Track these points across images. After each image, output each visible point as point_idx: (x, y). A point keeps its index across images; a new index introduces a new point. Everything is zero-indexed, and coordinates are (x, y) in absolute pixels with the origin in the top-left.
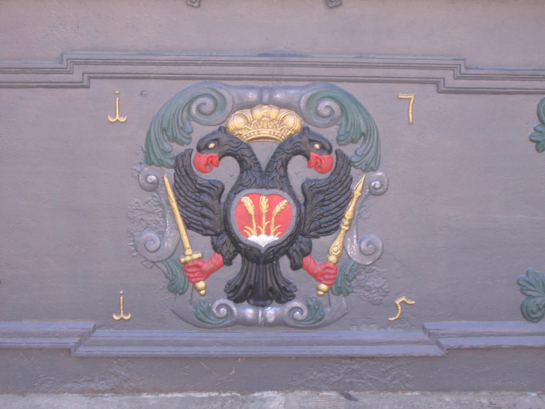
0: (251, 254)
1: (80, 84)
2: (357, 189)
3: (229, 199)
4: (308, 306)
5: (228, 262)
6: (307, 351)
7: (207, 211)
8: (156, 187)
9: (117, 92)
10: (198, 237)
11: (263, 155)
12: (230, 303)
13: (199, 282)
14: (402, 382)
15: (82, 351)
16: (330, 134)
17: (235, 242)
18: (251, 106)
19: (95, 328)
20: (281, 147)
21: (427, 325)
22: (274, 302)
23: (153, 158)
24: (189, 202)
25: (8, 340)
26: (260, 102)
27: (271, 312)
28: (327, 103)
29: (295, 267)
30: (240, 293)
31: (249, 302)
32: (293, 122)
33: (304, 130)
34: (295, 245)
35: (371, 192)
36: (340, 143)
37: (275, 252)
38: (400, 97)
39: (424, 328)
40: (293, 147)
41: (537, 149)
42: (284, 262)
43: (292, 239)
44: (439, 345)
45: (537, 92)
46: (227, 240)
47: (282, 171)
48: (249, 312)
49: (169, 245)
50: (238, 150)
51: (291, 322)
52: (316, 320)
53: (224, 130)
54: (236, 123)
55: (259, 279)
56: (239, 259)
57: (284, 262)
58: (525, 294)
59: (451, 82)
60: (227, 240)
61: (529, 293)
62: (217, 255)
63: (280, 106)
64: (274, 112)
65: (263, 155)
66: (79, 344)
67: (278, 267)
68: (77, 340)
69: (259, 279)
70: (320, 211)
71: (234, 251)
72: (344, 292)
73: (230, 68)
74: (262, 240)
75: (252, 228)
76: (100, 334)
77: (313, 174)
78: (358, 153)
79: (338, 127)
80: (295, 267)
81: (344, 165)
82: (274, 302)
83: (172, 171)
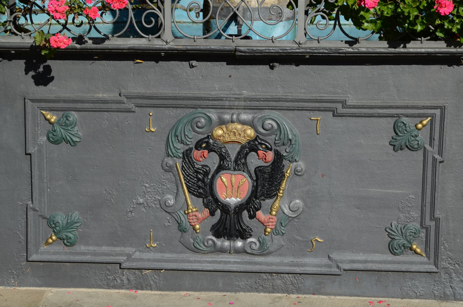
0: (225, 208)
3: (213, 177)
4: (259, 241)
7: (203, 186)
9: (151, 114)
12: (214, 238)
16: (271, 139)
17: (216, 200)
20: (243, 147)
21: (334, 256)
22: (239, 238)
23: (170, 153)
24: (190, 178)
28: (270, 122)
29: (252, 217)
30: (219, 231)
31: (224, 238)
32: (250, 132)
34: (250, 206)
35: (296, 173)
36: (277, 145)
37: (240, 208)
38: (312, 118)
39: (329, 257)
40: (253, 146)
41: (394, 150)
42: (245, 214)
44: (338, 267)
45: (392, 116)
46: (212, 202)
47: (243, 160)
48: (227, 244)
51: (249, 251)
52: (263, 251)
55: (230, 224)
58: (391, 238)
60: (212, 202)
61: (392, 237)
62: (206, 209)
63: (243, 123)
70: (267, 182)
71: (216, 207)
72: (281, 234)
74: (233, 200)
77: (261, 163)
78: (287, 151)
79: (275, 136)
80: (252, 217)
82: (239, 238)
83: (182, 160)
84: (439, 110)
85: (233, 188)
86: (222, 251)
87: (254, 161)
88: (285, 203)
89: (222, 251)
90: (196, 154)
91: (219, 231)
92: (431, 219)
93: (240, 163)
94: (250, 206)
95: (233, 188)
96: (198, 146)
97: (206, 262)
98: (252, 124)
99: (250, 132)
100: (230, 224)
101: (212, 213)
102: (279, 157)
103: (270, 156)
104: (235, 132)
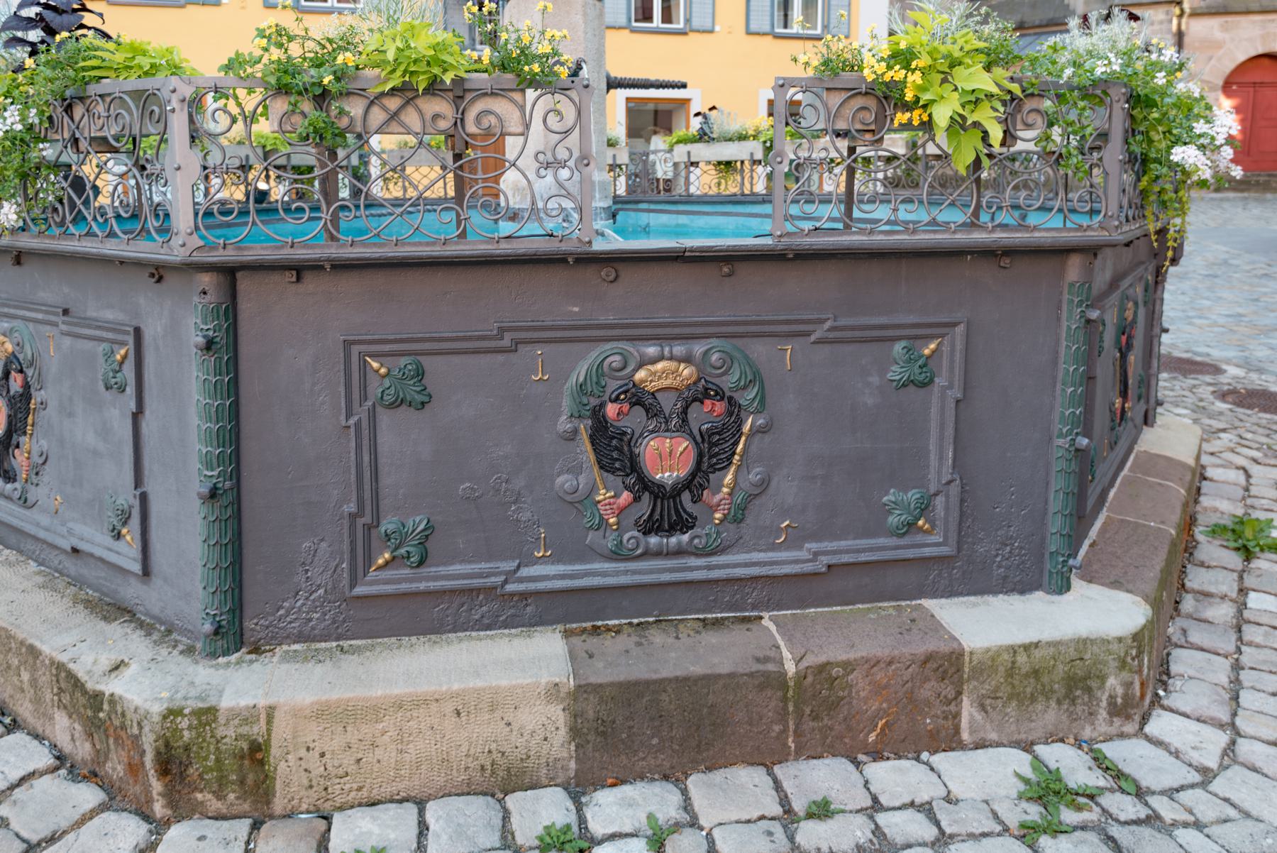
1: (493, 344)
2: (746, 428)
7: (616, 453)
10: (611, 477)
15: (510, 587)
18: (654, 361)
19: (519, 567)
25: (957, 378)
26: (661, 358)
32: (687, 371)
34: (696, 482)
40: (702, 392)
42: (686, 496)
43: (693, 475)
50: (637, 397)
56: (646, 497)
57: (686, 496)
64: (673, 365)
65: (668, 403)
66: (506, 582)
67: (1160, 287)
68: (503, 578)
69: (667, 511)
70: (713, 451)
73: (1130, 382)
76: (524, 572)
80: (696, 500)
81: (735, 410)
83: (590, 422)
85: (666, 457)
89: (648, 554)
90: (611, 410)
94: (696, 482)
98: (687, 360)
99: (687, 371)
100: (667, 511)
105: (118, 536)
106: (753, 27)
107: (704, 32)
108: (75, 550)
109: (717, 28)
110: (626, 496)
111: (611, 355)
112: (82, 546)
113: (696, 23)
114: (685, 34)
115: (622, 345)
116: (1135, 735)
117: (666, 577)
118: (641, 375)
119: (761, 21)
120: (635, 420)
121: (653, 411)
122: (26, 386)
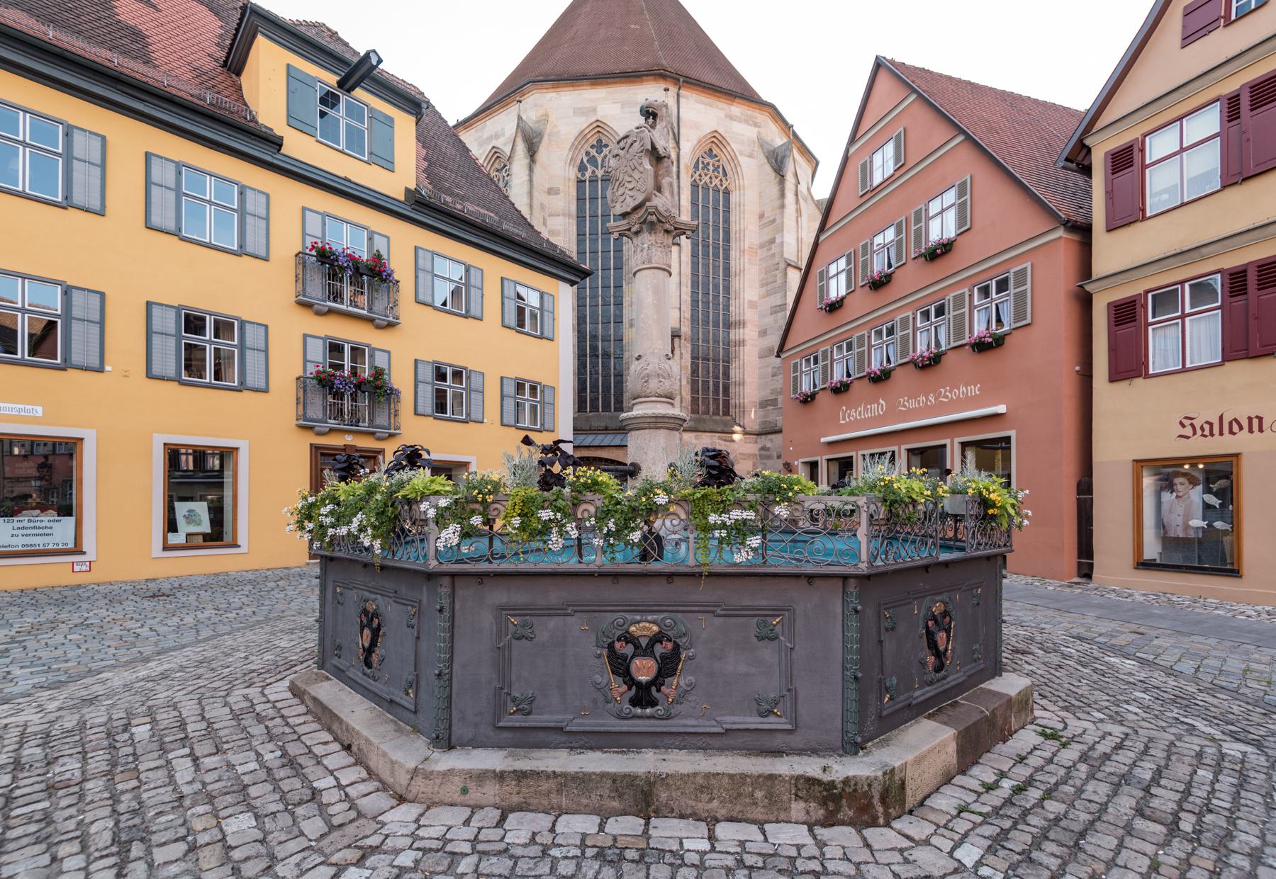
0: (639, 685)
2: (683, 657)
5: (630, 689)
6: (664, 730)
7: (621, 667)
8: (599, 656)
11: (644, 642)
13: (778, 503)
14: (211, 799)
15: (568, 729)
17: (632, 679)
18: (638, 622)
27: (648, 711)
30: (635, 702)
32: (655, 628)
33: (660, 632)
34: (657, 682)
40: (657, 639)
42: (653, 689)
43: (656, 678)
48: (639, 711)
49: (605, 682)
53: (627, 632)
54: (633, 628)
57: (653, 689)
59: (719, 611)
65: (644, 642)
70: (668, 666)
74: (643, 678)
75: (1189, 39)
80: (659, 691)
84: (177, 504)
85: (644, 670)
86: (636, 717)
87: (659, 649)
88: (679, 681)
89: (636, 717)
90: (617, 645)
91: (635, 702)
92: (188, 535)
93: (648, 651)
94: (657, 682)
95: (644, 670)
96: (619, 640)
97: (625, 726)
98: (654, 622)
99: (655, 628)
100: (643, 696)
101: (630, 689)
102: (677, 647)
103: (670, 645)
104: (644, 628)
105: (407, 694)
106: (505, 422)
107: (87, 369)
108: (392, 701)
109: (108, 368)
110: (625, 687)
111: (618, 618)
112: (395, 698)
113: (473, 416)
114: (64, 369)
115: (672, 615)
116: (444, 873)
117: (659, 729)
118: (633, 628)
119: (510, 419)
120: (629, 650)
121: (637, 646)
122: (379, 625)
